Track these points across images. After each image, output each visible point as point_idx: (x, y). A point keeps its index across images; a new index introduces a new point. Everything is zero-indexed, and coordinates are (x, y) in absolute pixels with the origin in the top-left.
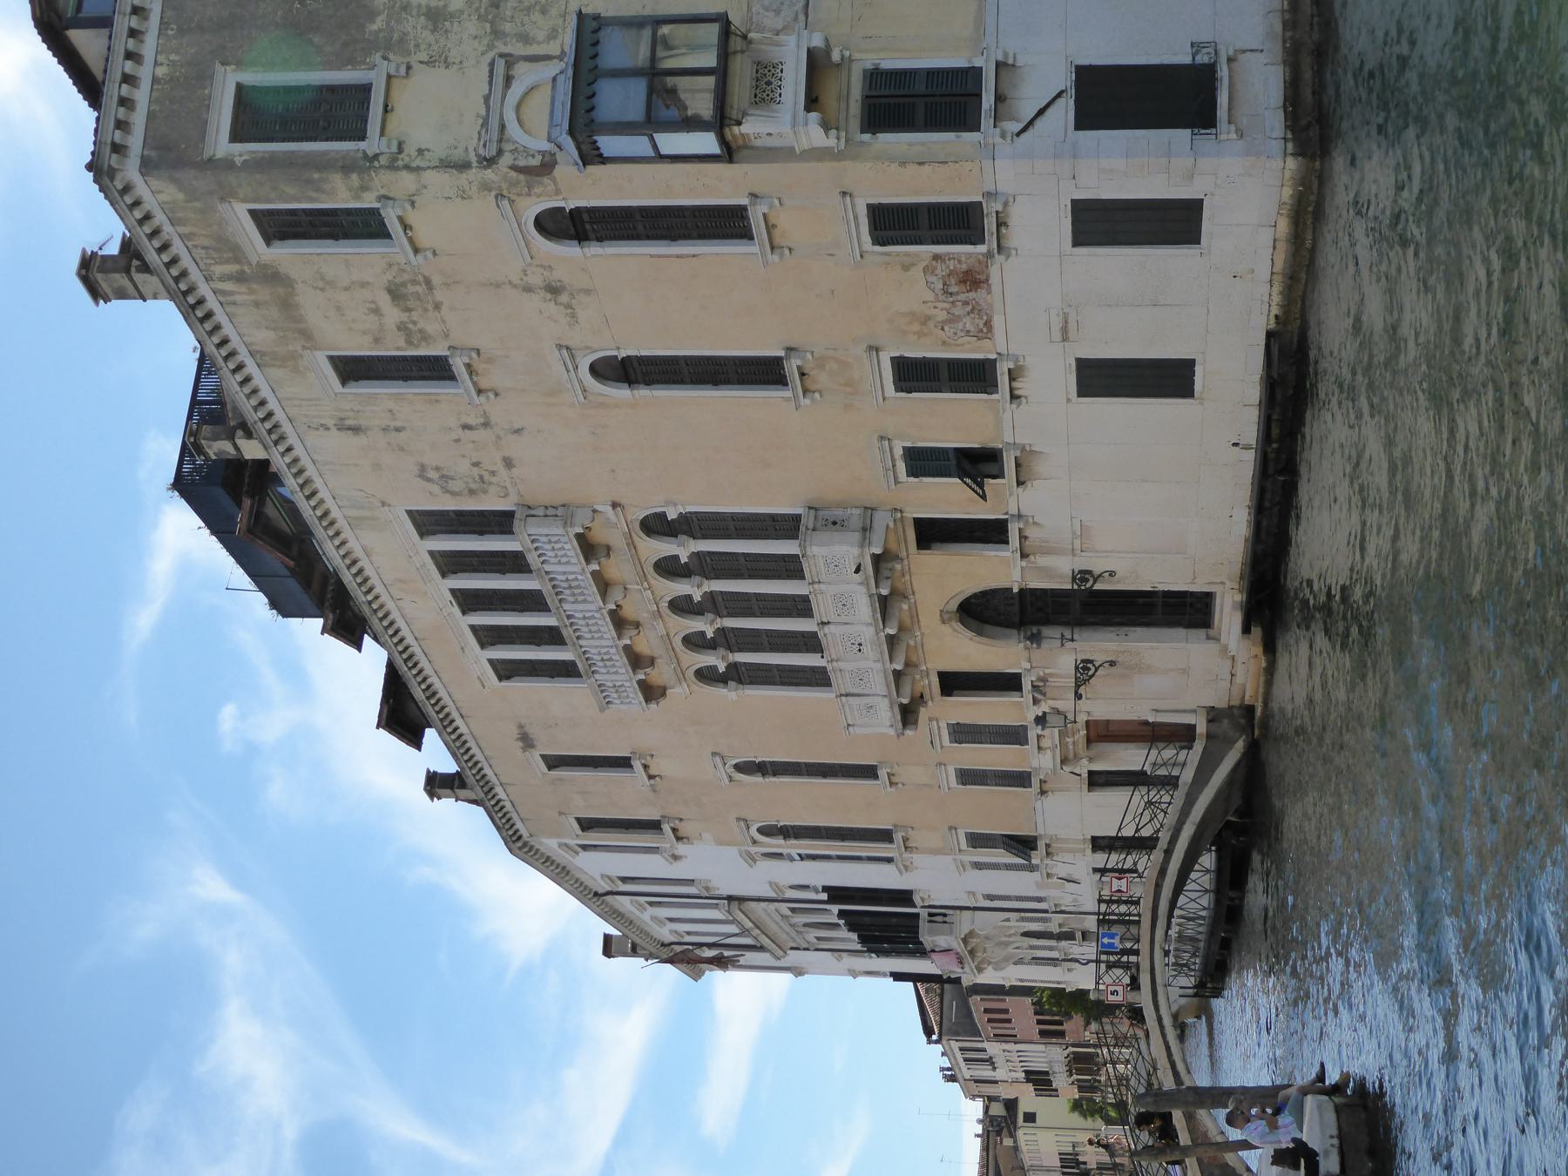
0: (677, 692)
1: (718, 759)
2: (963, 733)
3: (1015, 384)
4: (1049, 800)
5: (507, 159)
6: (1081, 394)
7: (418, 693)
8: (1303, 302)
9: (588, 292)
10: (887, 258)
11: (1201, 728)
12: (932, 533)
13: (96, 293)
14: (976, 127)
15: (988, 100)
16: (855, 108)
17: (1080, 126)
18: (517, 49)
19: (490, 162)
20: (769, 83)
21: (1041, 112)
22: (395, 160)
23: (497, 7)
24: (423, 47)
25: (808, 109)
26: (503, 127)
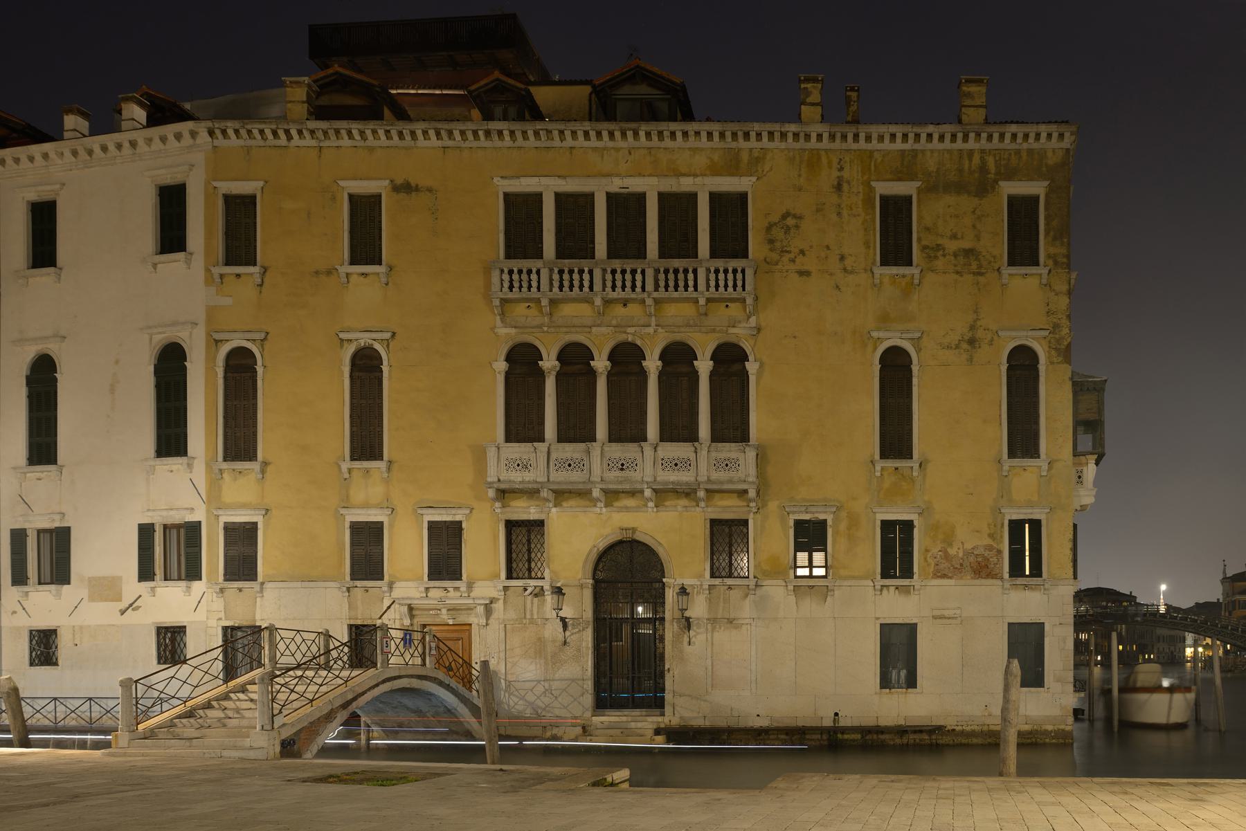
1: (387, 335)
8: (921, 731)
9: (971, 360)
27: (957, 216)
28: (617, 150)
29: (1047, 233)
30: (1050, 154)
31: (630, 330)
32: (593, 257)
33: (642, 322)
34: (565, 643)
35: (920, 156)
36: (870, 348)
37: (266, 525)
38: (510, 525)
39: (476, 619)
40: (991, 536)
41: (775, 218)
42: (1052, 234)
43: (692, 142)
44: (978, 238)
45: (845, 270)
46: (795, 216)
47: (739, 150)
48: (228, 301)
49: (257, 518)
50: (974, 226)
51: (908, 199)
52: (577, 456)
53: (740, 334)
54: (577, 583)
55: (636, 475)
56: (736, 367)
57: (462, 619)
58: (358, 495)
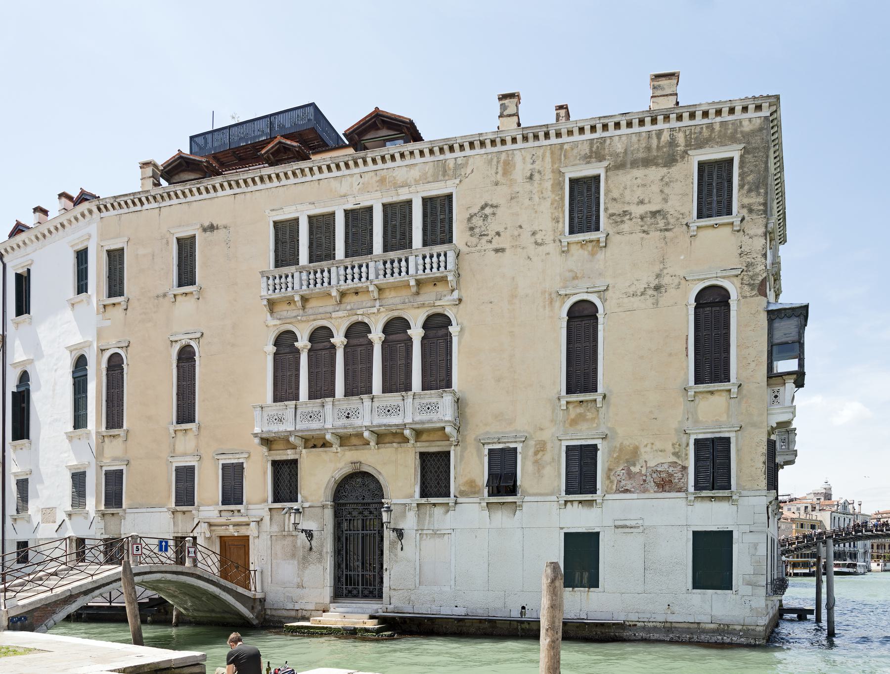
1: (198, 335)
3: (575, 504)
4: (169, 515)
6: (567, 536)
7: (393, 148)
10: (684, 445)
27: (644, 185)
28: (352, 175)
29: (741, 186)
30: (746, 123)
31: (359, 312)
32: (334, 258)
33: (369, 305)
34: (311, 549)
35: (608, 142)
36: (557, 304)
37: (128, 471)
38: (275, 463)
39: (251, 531)
40: (676, 454)
41: (475, 210)
42: (746, 187)
43: (408, 161)
44: (666, 200)
45: (536, 243)
46: (492, 206)
47: (446, 160)
48: (108, 323)
49: (124, 467)
50: (662, 191)
51: (597, 178)
52: (316, 409)
53: (445, 305)
54: (320, 505)
55: (357, 422)
56: (441, 332)
57: (243, 531)
58: (180, 447)
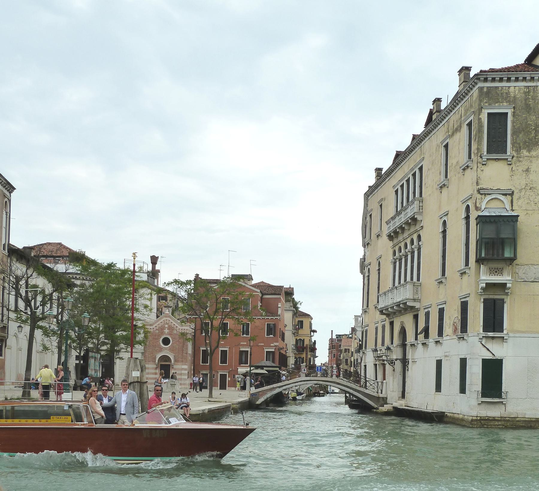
0: (391, 244)
2: (384, 327)
5: (479, 196)
11: (381, 395)
12: (416, 317)
13: (460, 71)
14: (484, 331)
15: (491, 334)
16: (491, 297)
17: (484, 360)
18: (515, 197)
19: (479, 191)
20: (496, 272)
21: (488, 350)
22: (480, 163)
23: (530, 189)
24: (517, 168)
25: (486, 283)
26: (490, 194)
